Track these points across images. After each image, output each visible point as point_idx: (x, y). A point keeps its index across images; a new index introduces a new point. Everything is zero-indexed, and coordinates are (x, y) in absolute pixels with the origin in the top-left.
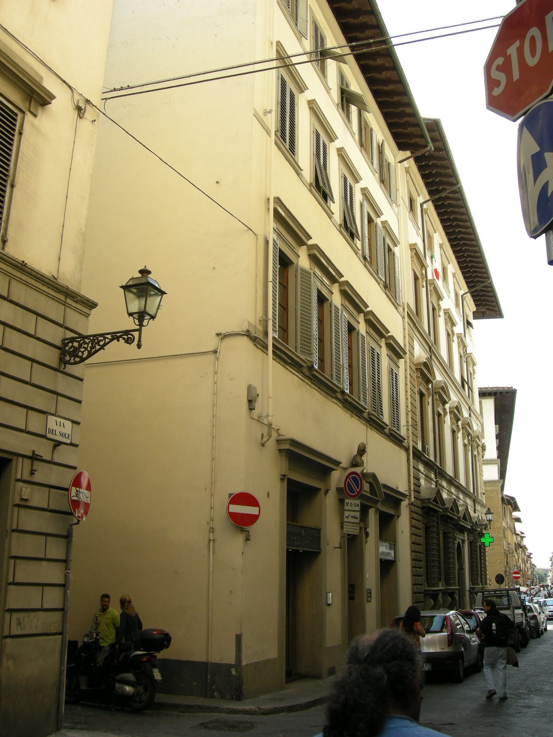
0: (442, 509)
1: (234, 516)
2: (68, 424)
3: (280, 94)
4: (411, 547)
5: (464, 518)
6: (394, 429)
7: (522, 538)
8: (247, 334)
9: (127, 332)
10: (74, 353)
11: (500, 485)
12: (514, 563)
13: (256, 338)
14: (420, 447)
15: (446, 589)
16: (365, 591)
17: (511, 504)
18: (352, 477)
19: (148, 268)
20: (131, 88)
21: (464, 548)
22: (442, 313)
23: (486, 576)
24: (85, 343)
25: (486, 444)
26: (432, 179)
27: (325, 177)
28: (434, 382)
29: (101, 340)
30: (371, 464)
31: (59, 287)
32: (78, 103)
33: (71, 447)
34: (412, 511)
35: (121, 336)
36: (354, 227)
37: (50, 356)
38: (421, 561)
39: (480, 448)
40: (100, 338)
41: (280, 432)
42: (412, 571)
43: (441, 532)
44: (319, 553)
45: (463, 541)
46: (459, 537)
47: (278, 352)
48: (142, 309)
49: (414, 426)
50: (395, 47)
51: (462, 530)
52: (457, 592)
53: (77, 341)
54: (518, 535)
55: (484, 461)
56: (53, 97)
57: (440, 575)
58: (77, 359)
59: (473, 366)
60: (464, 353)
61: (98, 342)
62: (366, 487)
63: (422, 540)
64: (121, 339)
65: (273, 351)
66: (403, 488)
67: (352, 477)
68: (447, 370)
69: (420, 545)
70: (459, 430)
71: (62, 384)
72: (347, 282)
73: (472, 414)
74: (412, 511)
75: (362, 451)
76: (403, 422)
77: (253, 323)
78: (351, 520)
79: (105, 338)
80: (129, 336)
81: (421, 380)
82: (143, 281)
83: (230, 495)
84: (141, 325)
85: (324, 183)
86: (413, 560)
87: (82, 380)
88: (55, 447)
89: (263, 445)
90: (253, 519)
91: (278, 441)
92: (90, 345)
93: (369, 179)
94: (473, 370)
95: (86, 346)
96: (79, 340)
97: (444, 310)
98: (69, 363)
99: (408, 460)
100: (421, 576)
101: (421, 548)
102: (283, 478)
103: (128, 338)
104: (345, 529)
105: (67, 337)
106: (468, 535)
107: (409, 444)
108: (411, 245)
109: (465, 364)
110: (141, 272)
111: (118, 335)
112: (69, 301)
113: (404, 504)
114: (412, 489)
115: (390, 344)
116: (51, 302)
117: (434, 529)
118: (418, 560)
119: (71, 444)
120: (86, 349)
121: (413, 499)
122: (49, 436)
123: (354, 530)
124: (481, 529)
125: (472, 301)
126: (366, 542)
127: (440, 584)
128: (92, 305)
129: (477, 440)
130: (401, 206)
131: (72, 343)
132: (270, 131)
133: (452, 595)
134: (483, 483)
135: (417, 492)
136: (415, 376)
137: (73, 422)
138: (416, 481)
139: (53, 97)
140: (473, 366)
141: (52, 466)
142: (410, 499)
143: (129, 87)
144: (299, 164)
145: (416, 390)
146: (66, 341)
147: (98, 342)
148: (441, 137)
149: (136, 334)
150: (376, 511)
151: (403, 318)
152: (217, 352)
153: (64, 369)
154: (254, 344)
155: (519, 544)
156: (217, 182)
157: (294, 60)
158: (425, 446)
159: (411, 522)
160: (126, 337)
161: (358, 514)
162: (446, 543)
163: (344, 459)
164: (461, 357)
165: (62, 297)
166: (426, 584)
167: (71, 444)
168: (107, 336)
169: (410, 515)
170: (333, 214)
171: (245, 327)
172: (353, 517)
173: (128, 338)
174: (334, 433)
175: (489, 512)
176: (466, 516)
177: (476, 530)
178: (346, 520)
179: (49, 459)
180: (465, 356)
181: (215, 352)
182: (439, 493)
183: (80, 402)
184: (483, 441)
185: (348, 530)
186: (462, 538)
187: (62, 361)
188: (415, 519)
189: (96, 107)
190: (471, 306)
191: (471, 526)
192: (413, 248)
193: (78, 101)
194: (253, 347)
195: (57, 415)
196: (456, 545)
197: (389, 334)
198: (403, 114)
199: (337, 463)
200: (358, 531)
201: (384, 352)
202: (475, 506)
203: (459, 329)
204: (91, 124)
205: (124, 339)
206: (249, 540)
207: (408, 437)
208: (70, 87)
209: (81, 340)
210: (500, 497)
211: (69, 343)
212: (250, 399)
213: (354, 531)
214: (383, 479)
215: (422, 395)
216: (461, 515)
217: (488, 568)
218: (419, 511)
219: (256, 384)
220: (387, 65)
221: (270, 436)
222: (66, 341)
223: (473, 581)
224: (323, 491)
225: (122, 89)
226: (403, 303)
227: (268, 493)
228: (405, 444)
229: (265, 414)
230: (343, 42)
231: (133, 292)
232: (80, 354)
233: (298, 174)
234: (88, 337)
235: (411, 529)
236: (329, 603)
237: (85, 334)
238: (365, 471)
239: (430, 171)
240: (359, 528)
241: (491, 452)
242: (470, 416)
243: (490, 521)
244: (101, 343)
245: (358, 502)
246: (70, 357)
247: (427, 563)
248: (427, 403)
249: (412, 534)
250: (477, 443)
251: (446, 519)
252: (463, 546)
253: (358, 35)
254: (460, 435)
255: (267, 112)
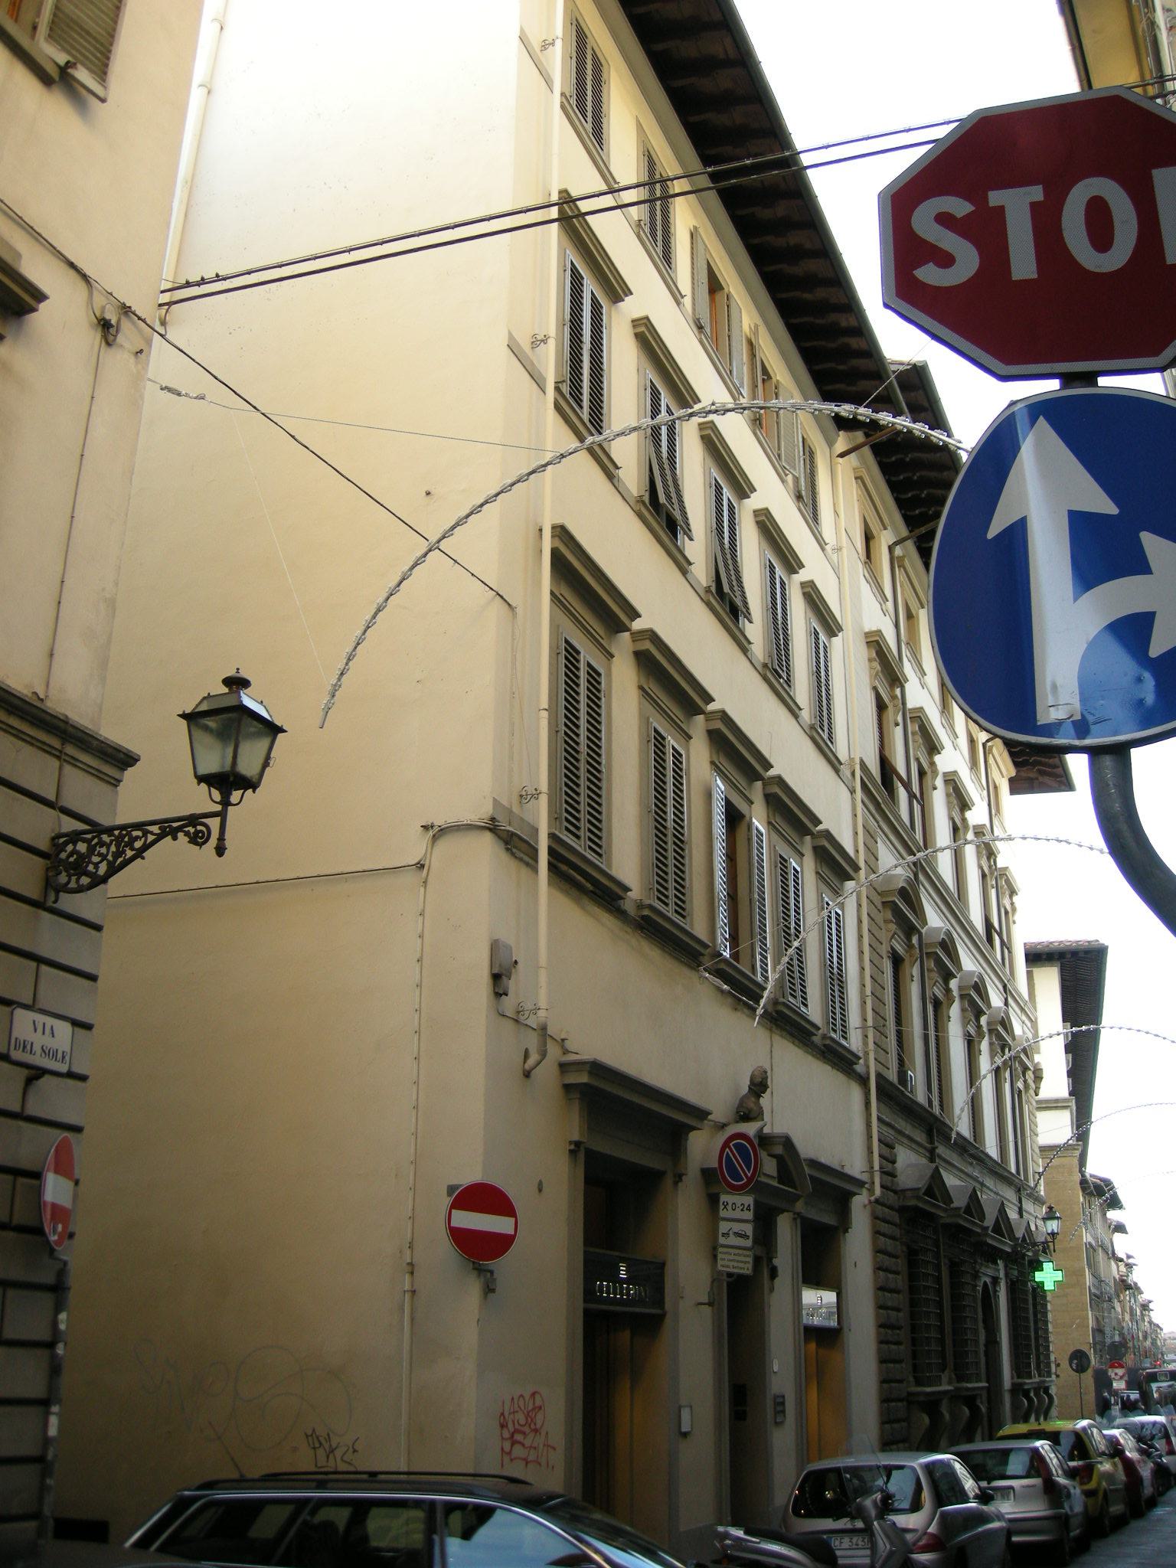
0: (945, 1210)
1: (462, 1238)
2: (64, 1029)
3: (568, 304)
4: (876, 1297)
5: (997, 1229)
6: (833, 1035)
7: (1129, 1266)
8: (492, 826)
9: (193, 820)
10: (78, 867)
11: (1077, 1153)
12: (1114, 1323)
13: (513, 834)
14: (892, 1076)
15: (957, 1389)
16: (769, 1403)
17: (1102, 1194)
18: (738, 1146)
19: (244, 674)
20: (225, 279)
21: (997, 1297)
22: (939, 782)
23: (1048, 1356)
24: (102, 844)
25: (1043, 1066)
26: (899, 456)
27: (670, 483)
28: (923, 931)
29: (137, 838)
30: (781, 1115)
31: (48, 718)
32: (103, 312)
33: (71, 1082)
34: (876, 1218)
35: (180, 829)
36: (738, 593)
37: (25, 874)
38: (900, 1328)
39: (1030, 1075)
40: (135, 833)
41: (567, 1044)
42: (879, 1351)
43: (944, 1262)
44: (661, 1318)
45: (995, 1281)
46: (987, 1273)
47: (564, 867)
48: (227, 768)
49: (880, 1029)
50: (808, 171)
51: (992, 1255)
52: (984, 1394)
53: (84, 841)
54: (1121, 1260)
55: (1038, 1102)
56: (40, 297)
57: (944, 1357)
58: (85, 880)
59: (1011, 897)
60: (990, 867)
61: (129, 842)
62: (770, 1166)
63: (900, 1281)
64: (180, 835)
65: (549, 863)
66: (856, 1167)
67: (738, 1146)
68: (953, 904)
69: (897, 1292)
70: (981, 1035)
71: (49, 937)
72: (724, 712)
73: (1010, 1000)
74: (876, 1218)
75: (759, 1086)
76: (854, 1019)
77: (505, 802)
78: (733, 1240)
79: (146, 833)
80: (199, 828)
81: (893, 927)
82: (230, 702)
83: (451, 1189)
84: (226, 803)
85: (669, 497)
86: (881, 1326)
87: (98, 928)
88: (29, 1081)
89: (527, 1074)
90: (500, 1244)
91: (564, 1067)
92: (113, 848)
93: (771, 492)
94: (1012, 904)
95: (104, 850)
96: (89, 836)
97: (945, 774)
98: (65, 889)
99: (867, 1104)
100: (900, 1362)
101: (900, 1300)
102: (576, 1149)
103: (197, 832)
104: (720, 1263)
105: (64, 830)
106: (1006, 1267)
107: (868, 1067)
108: (867, 634)
109: (993, 892)
110: (229, 682)
111: (175, 825)
112: (70, 750)
113: (859, 1204)
114: (877, 1167)
115: (823, 848)
116: (28, 750)
117: (929, 1257)
118: (892, 1327)
119: (71, 1075)
120: (104, 857)
121: (878, 1191)
122: (16, 1055)
123: (743, 1265)
124: (1036, 1253)
125: (1006, 754)
126: (772, 1289)
127: (945, 1377)
128: (125, 760)
129: (1023, 1056)
130: (845, 550)
131: (75, 844)
132: (545, 380)
133: (970, 1401)
134: (1037, 1150)
135: (889, 1173)
136: (879, 918)
137: (76, 1023)
138: (886, 1151)
139: (40, 297)
140: (1011, 897)
141: (21, 1123)
142: (871, 1191)
143: (218, 278)
144: (613, 456)
145: (884, 950)
146: (62, 840)
147: (129, 842)
148: (929, 401)
149: (214, 823)
150: (795, 1219)
151: (852, 792)
152: (423, 866)
153: (56, 901)
154: (507, 849)
155: (1123, 1281)
156: (428, 494)
157: (584, 206)
158: (905, 1073)
159: (874, 1242)
160: (191, 830)
161: (748, 1229)
162: (955, 1285)
163: (719, 1100)
164: (984, 876)
165: (55, 743)
166: (911, 1379)
167: (71, 1075)
168: (150, 828)
169: (874, 1225)
170: (690, 564)
171: (480, 812)
172: (738, 1235)
173: (197, 832)
174: (692, 1047)
175: (1050, 1216)
176: (1003, 1225)
177: (1025, 1255)
178: (722, 1240)
179: (16, 1107)
180: (992, 873)
181: (420, 866)
182: (936, 1176)
183: (92, 978)
184: (1037, 1058)
185: (726, 1263)
186: (990, 1272)
187: (50, 885)
188: (884, 1235)
189: (144, 321)
190: (1002, 767)
191: (1014, 1248)
192: (875, 643)
193: (103, 308)
194: (504, 856)
195: (40, 1005)
196: (980, 1289)
197: (820, 827)
198: (848, 353)
199: (702, 1114)
200: (750, 1266)
201: (806, 868)
202: (1020, 1201)
203: (977, 815)
204: (132, 359)
205: (187, 834)
206: (493, 1291)
207: (866, 1053)
208: (85, 277)
209: (93, 838)
210: (1078, 1177)
211: (66, 843)
212: (496, 971)
213: (741, 1265)
214: (806, 1148)
215: (897, 961)
216: (989, 1222)
217: (1052, 1338)
218: (895, 1217)
219: (507, 937)
220: (808, 246)
221: (543, 1054)
222: (62, 840)
223: (1020, 1368)
224: (669, 1180)
225: (203, 281)
226: (852, 760)
227: (540, 1184)
228: (859, 1068)
229: (529, 1006)
230: (695, 164)
231: (206, 728)
232: (91, 868)
233: (610, 477)
234: (109, 831)
235: (875, 1257)
236: (684, 1430)
237: (106, 821)
238: (766, 1130)
239: (899, 456)
240: (750, 1260)
241: (1056, 1082)
242: (1006, 1004)
243: (1053, 1234)
244: (138, 844)
245: (749, 1200)
246: (69, 876)
247: (914, 1345)
248: (908, 977)
249: (878, 1268)
250: (1022, 1063)
251: (957, 1233)
252: (995, 1291)
253: (728, 150)
254: (984, 1046)
255: (538, 342)
